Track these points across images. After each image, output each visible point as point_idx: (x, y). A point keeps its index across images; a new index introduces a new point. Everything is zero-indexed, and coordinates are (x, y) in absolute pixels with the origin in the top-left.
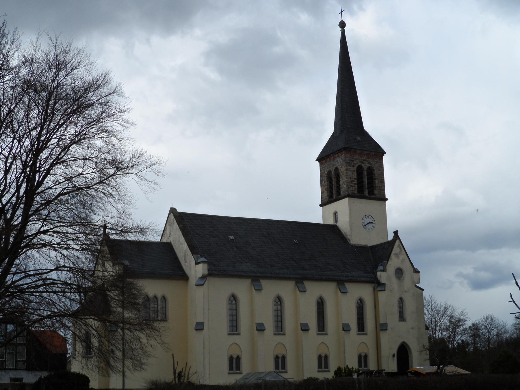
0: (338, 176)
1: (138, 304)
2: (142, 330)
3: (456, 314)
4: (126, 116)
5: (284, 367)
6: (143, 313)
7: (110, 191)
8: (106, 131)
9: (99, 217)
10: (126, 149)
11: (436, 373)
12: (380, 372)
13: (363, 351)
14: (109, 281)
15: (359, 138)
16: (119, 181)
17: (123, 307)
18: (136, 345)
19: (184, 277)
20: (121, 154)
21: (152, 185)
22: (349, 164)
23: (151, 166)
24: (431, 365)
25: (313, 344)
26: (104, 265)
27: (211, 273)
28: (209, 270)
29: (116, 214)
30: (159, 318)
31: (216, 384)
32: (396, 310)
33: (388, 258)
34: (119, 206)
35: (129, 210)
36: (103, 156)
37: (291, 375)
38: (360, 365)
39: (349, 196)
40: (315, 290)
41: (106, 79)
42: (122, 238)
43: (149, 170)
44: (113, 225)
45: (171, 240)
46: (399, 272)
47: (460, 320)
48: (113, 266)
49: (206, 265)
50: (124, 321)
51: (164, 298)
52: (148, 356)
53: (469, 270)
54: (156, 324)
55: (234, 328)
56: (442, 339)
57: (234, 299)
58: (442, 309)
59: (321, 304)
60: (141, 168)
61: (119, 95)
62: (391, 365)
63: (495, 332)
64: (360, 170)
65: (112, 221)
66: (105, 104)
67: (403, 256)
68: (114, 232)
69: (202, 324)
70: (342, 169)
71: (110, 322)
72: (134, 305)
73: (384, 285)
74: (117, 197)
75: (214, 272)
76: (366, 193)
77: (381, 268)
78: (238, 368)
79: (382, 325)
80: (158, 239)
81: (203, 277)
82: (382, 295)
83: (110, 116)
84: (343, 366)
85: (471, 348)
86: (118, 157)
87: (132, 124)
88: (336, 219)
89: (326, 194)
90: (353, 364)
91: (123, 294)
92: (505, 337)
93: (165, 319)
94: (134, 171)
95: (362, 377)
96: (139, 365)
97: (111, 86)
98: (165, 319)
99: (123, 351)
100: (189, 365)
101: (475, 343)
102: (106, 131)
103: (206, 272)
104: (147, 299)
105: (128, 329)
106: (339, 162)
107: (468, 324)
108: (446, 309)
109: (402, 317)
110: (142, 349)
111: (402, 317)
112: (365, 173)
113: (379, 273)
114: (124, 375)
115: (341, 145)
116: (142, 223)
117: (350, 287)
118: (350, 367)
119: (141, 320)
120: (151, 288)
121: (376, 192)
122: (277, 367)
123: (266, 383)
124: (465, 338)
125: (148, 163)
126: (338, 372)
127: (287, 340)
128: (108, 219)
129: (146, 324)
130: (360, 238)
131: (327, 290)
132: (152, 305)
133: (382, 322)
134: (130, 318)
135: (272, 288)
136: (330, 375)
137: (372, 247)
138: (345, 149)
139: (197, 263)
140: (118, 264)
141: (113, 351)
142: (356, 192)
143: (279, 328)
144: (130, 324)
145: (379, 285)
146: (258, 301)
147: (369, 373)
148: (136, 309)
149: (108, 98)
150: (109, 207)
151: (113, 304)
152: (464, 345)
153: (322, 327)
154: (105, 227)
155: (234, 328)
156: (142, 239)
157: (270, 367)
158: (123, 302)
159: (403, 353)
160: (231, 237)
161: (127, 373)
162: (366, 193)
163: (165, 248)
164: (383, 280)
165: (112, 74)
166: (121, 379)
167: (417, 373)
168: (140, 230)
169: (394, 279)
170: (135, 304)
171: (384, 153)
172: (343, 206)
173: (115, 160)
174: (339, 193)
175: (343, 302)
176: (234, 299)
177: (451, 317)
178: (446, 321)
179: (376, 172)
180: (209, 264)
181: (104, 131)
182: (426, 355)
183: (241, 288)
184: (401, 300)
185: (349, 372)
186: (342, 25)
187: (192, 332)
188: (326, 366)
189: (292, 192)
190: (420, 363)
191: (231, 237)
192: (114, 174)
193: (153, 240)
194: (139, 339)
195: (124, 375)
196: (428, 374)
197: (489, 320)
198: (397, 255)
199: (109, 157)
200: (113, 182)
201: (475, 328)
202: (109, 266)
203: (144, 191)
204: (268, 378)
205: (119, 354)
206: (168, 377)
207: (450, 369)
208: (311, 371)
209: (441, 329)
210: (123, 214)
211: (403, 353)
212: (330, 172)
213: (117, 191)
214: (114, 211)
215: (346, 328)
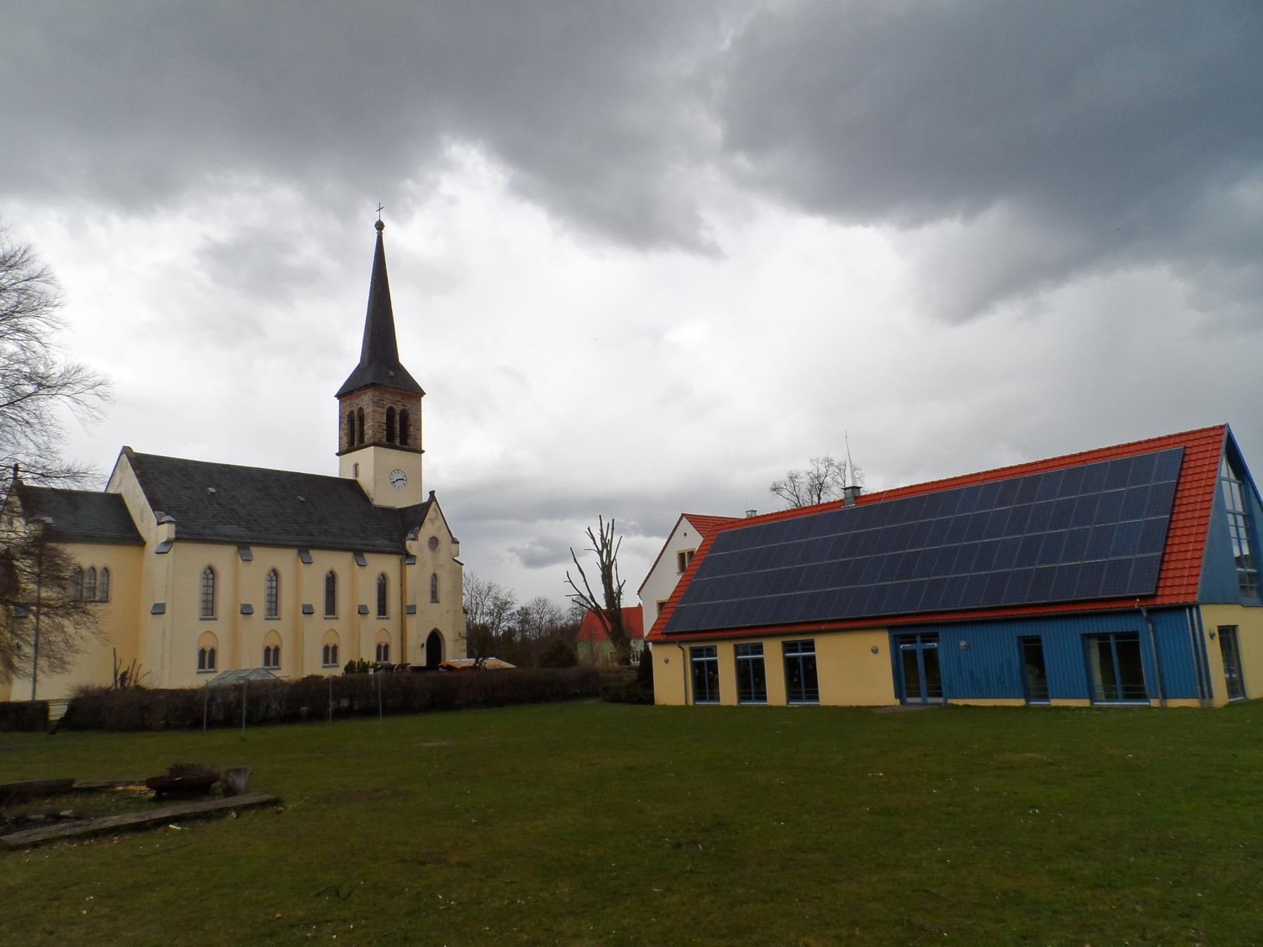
0: (362, 419)
1: (64, 579)
2: (67, 614)
3: (502, 596)
4: (56, 312)
5: (276, 662)
6: (71, 591)
7: (27, 417)
8: (24, 331)
9: (6, 454)
10: (55, 359)
11: (473, 668)
12: (403, 666)
13: (383, 640)
14: (17, 546)
15: (391, 373)
16: (41, 404)
17: (40, 583)
18: (56, 637)
19: (139, 541)
20: (46, 365)
21: (95, 413)
22: (377, 404)
23: (93, 387)
24: (469, 656)
25: (318, 630)
26: (11, 523)
27: (180, 537)
28: (177, 532)
29: (33, 450)
30: (97, 598)
31: (178, 687)
32: (428, 589)
33: (421, 524)
34: (40, 440)
35: (55, 446)
36: (16, 366)
37: (287, 672)
38: (378, 658)
39: (374, 444)
40: (324, 561)
41: (26, 256)
42: (42, 486)
43: (91, 391)
44: (28, 465)
45: (120, 490)
46: (434, 542)
47: (506, 603)
48: (27, 524)
49: (173, 526)
50: (39, 603)
51: (106, 570)
52: (76, 652)
53: (524, 544)
54: (90, 607)
55: (209, 609)
56: (484, 626)
57: (211, 572)
58: (486, 588)
59: (331, 580)
60: (78, 388)
61: (47, 282)
62: (418, 658)
63: (547, 617)
64: (390, 413)
65: (27, 460)
66: (23, 291)
67: (439, 523)
68: (29, 475)
69: (163, 605)
70: (368, 410)
71: (15, 604)
72: (58, 581)
73: (414, 557)
74: (38, 426)
75: (185, 535)
76: (397, 442)
77: (411, 536)
78: (212, 665)
79: (409, 607)
80: (101, 489)
81: (168, 543)
82: (410, 570)
83: (32, 310)
84: (356, 660)
85: (518, 638)
86: (42, 369)
87: (66, 325)
88: (356, 474)
89: (345, 440)
90: (369, 657)
91: (40, 564)
92: (560, 623)
93: (105, 600)
94: (66, 391)
95: (380, 673)
96: (60, 664)
97: (36, 267)
98: (105, 600)
99: (36, 646)
100: (138, 663)
101: (523, 631)
102: (24, 331)
103: (173, 536)
104: (80, 571)
105: (45, 614)
106: (366, 401)
107: (516, 608)
108: (490, 589)
109: (435, 598)
110: (67, 642)
111: (435, 598)
112: (398, 417)
113: (408, 543)
114: (35, 680)
115: (369, 380)
116: (77, 464)
117: (370, 558)
118: (365, 660)
119: (66, 600)
120: (84, 556)
121: (409, 441)
122: (267, 662)
123: (250, 685)
124: (511, 624)
125: (91, 382)
126: (350, 667)
127: (283, 627)
128: (21, 457)
129: (75, 607)
130: (385, 497)
131: (340, 562)
132: (86, 580)
133: (409, 604)
134: (49, 599)
135: (265, 558)
136: (338, 672)
137: (401, 510)
138: (373, 385)
139: (159, 524)
140: (34, 522)
141: (19, 647)
142: (384, 440)
143: (273, 609)
144: (48, 606)
145: (407, 557)
146: (244, 574)
147: (390, 668)
148: (60, 586)
149: (28, 283)
150: (23, 441)
151: (23, 579)
152: (511, 632)
153: (331, 608)
154: (16, 468)
155: (209, 609)
156: (74, 487)
157: (259, 662)
158: (38, 575)
159: (434, 643)
160: (212, 490)
161: (41, 677)
162: (397, 442)
163: (114, 503)
164: (412, 552)
165: (34, 251)
166: (30, 687)
167: (450, 668)
168: (72, 474)
169: (427, 551)
170: (59, 578)
171: (423, 393)
172: (366, 457)
173: (37, 374)
174: (362, 440)
175: (359, 577)
176: (211, 572)
177: (496, 598)
178: (489, 604)
179: (412, 417)
180: (178, 524)
181: (18, 330)
182: (463, 645)
183: (222, 557)
184: (435, 577)
185: (364, 667)
186: (380, 226)
187: (146, 616)
188: (335, 660)
189: (301, 436)
190: (455, 656)
191: (212, 490)
192: (34, 393)
193: (92, 489)
194: (61, 628)
195: (35, 680)
196: (464, 668)
197: (542, 603)
198: (432, 521)
199: (26, 369)
200: (30, 405)
201: (525, 613)
202: (19, 524)
203: (82, 420)
204: (253, 678)
205: (28, 650)
206: (103, 679)
207: (492, 662)
208: (313, 666)
209: (482, 613)
210: (45, 450)
211: (434, 643)
212: (352, 412)
213: (37, 417)
214: (31, 445)
215: (363, 611)
